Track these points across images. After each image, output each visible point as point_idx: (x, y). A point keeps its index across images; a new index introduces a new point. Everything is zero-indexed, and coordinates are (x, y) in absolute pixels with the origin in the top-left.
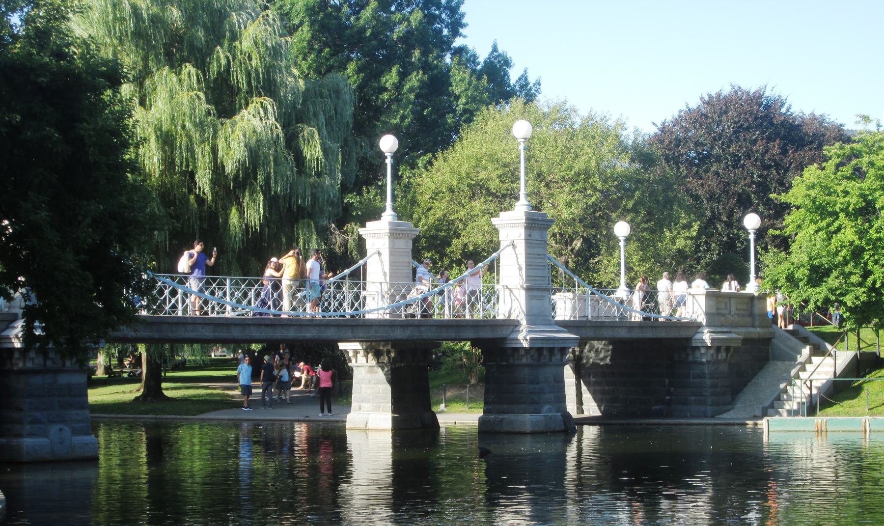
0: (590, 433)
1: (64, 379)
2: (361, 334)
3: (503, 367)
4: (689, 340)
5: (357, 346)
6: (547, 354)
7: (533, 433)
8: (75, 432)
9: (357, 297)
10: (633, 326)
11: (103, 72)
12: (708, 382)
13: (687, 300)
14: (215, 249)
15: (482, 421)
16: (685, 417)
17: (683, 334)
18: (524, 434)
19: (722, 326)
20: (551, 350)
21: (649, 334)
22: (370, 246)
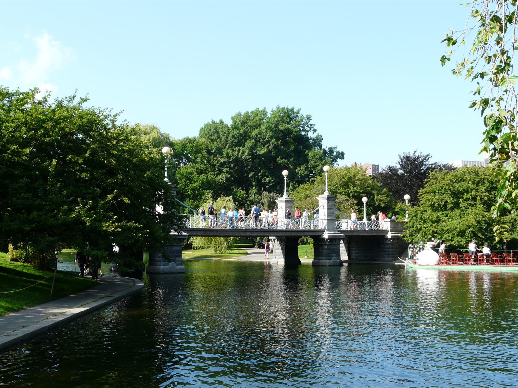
0: (345, 265)
1: (174, 248)
2: (276, 234)
3: (323, 246)
4: (384, 236)
5: (274, 238)
6: (334, 241)
7: (329, 266)
8: (178, 265)
9: (496, 260)
10: (365, 231)
11: (185, 231)
12: (391, 250)
13: (385, 224)
14: (144, 208)
15: (313, 262)
16: (382, 261)
17: (382, 234)
18: (326, 266)
19: (396, 232)
20: (335, 239)
21: (371, 234)
22: (320, 203)
